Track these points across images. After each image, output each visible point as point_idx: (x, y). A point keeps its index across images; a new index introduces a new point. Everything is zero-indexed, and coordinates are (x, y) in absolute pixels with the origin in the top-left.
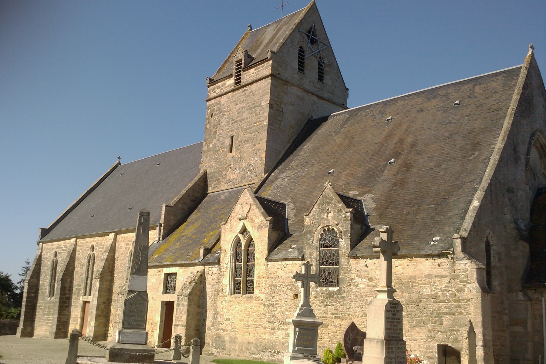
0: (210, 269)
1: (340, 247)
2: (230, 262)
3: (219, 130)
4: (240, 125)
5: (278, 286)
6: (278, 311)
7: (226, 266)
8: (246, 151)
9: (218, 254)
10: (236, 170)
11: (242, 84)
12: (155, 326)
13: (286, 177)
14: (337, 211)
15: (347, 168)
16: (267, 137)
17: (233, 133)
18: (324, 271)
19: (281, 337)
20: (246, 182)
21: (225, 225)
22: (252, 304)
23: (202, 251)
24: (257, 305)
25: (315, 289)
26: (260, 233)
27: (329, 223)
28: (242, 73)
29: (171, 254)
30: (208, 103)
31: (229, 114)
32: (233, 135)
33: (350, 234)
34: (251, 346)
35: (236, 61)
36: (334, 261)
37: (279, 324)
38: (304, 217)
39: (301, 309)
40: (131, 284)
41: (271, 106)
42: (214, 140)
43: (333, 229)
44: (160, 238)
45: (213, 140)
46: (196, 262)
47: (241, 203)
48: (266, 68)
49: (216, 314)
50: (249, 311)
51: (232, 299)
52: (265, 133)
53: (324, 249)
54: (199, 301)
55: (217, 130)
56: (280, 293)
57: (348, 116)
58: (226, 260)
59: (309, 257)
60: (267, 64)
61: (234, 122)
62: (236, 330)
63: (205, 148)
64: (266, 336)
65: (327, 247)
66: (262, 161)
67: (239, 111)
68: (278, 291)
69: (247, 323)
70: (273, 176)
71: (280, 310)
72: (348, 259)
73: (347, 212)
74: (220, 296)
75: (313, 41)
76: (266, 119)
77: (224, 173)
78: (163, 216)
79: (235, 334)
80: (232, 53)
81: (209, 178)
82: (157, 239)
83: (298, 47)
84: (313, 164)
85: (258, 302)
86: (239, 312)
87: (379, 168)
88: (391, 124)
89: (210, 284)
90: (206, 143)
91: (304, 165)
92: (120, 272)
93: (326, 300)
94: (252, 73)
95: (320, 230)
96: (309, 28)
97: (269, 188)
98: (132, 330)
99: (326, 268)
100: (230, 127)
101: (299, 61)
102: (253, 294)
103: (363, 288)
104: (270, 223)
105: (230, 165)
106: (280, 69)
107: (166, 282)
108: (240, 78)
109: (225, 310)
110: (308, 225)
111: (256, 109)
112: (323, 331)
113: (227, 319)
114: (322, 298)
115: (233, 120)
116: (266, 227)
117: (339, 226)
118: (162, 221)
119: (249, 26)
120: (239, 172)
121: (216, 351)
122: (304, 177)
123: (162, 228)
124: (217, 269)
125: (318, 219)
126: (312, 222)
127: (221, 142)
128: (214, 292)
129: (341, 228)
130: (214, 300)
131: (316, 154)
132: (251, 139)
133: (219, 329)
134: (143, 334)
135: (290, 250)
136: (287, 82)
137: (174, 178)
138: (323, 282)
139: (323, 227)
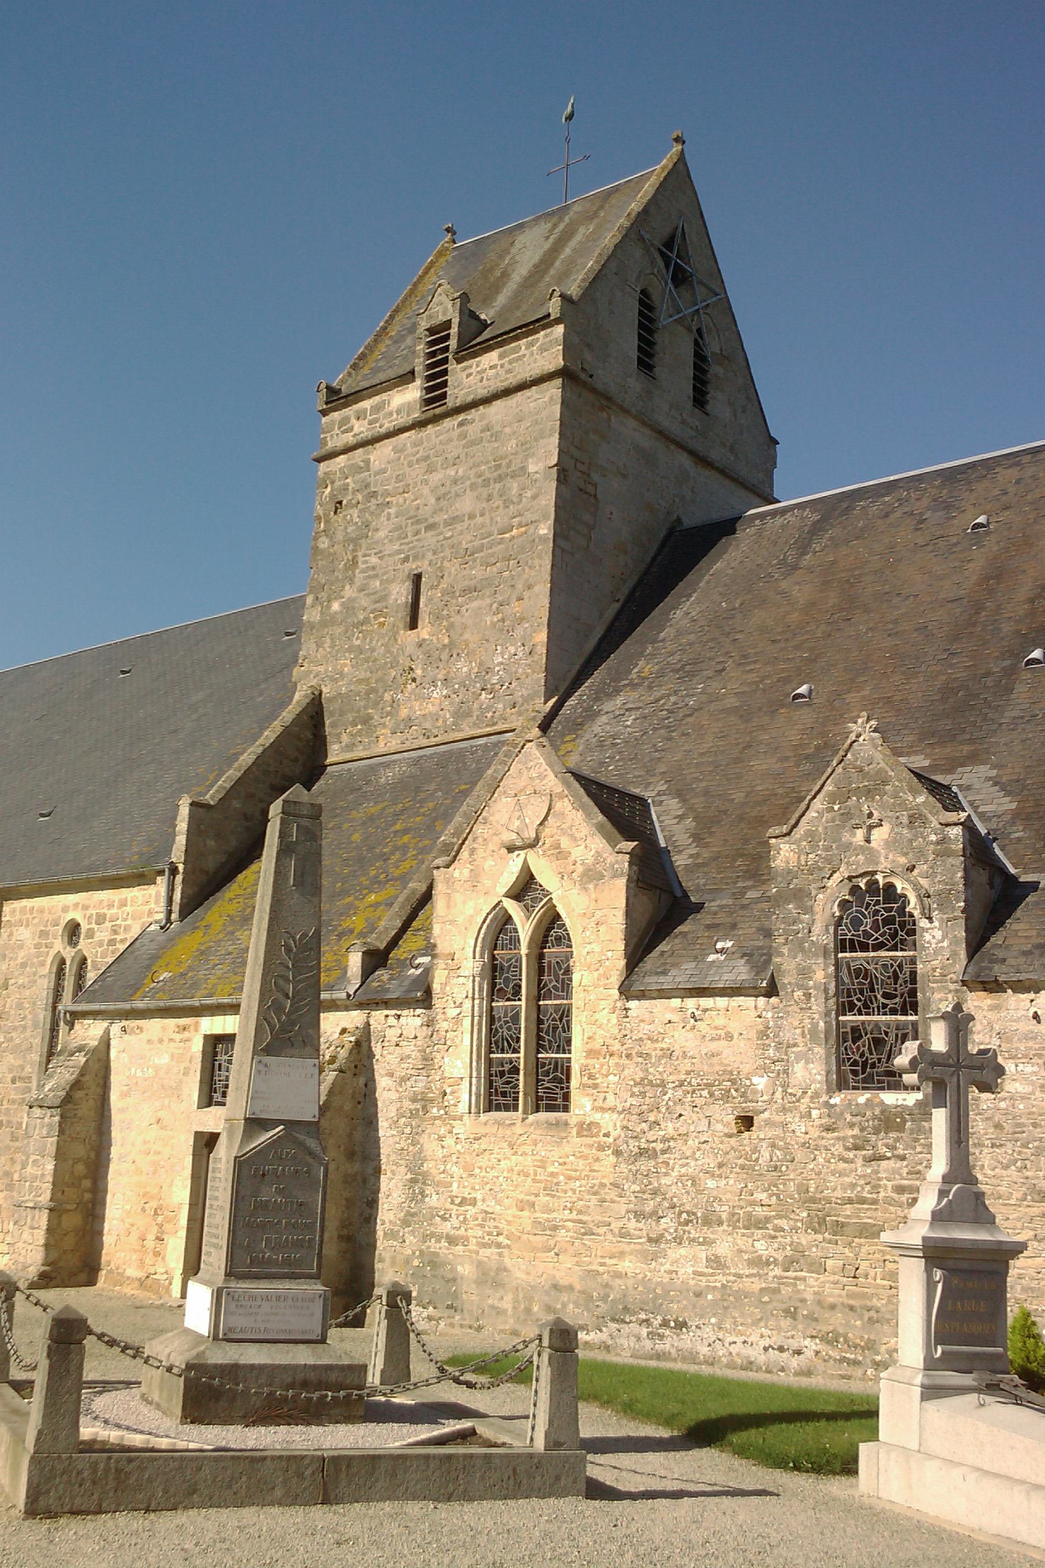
0: (392, 1021)
1: (924, 948)
2: (473, 999)
3: (365, 556)
4: (446, 539)
5: (671, 1085)
6: (675, 1174)
7: (458, 1010)
8: (470, 622)
9: (421, 970)
10: (435, 686)
11: (451, 402)
12: (174, 1220)
13: (627, 710)
14: (905, 820)
15: (862, 679)
16: (552, 575)
17: (423, 566)
18: (856, 1033)
19: (690, 1270)
20: (475, 725)
21: (448, 866)
22: (567, 1149)
23: (355, 961)
24: (586, 1151)
25: (825, 1098)
26: (593, 896)
27: (877, 864)
28: (452, 366)
29: (226, 968)
30: (323, 467)
31: (401, 500)
32: (420, 570)
33: (962, 904)
34: (565, 1299)
35: (426, 330)
36: (897, 1000)
37: (680, 1224)
38: (773, 841)
39: (942, 1193)
40: (255, 1092)
41: (562, 474)
42: (347, 587)
43: (890, 887)
44: (169, 912)
45: (343, 587)
46: (334, 996)
47: (512, 793)
48: (542, 350)
49: (418, 1180)
50: (552, 1174)
51: (482, 1130)
52: (545, 564)
53: (854, 954)
54: (351, 1133)
55: (360, 554)
56: (679, 1109)
57: (816, 517)
58: (456, 990)
59: (797, 985)
60: (546, 336)
61: (422, 526)
62: (501, 1239)
63: (312, 615)
64: (627, 1264)
65: (864, 948)
66: (536, 658)
67: (443, 490)
68: (671, 1103)
69: (546, 1216)
70: (574, 707)
71: (683, 1170)
72: (957, 991)
73: (947, 825)
74: (435, 1118)
75: (680, 278)
76: (545, 517)
77: (387, 697)
78: (181, 840)
79: (500, 1255)
80: (396, 311)
81: (332, 714)
82: (161, 916)
83: (638, 289)
84: (720, 667)
85: (590, 1141)
86: (515, 1177)
87: (989, 681)
88: (993, 538)
89: (391, 1075)
90: (317, 598)
91: (687, 671)
92: (15, 1029)
93: (873, 1138)
94: (491, 368)
95: (836, 886)
96: (667, 231)
97: (569, 746)
98: (264, 1284)
99: (863, 1022)
100: (408, 544)
101: (640, 336)
102: (566, 1109)
103: (1023, 1098)
104: (631, 863)
105: (412, 669)
106: (588, 356)
107: (209, 1066)
108: (445, 384)
109: (455, 1170)
110: (789, 872)
111: (508, 485)
112: (864, 1249)
113: (464, 1199)
114: (856, 1131)
115: (418, 522)
116: (614, 876)
117: (916, 872)
118: (178, 854)
119: (448, 230)
120: (445, 692)
121: (425, 1315)
122: (696, 710)
123: (179, 878)
124: (418, 1021)
125: (828, 849)
126: (803, 858)
127: (375, 593)
128: (407, 1104)
129: (924, 882)
130: (408, 1130)
131: (727, 635)
132: (490, 585)
133: (433, 1235)
134: (312, 1300)
135: (712, 957)
136: (609, 399)
137: (194, 716)
138: (855, 1073)
139: (850, 878)
